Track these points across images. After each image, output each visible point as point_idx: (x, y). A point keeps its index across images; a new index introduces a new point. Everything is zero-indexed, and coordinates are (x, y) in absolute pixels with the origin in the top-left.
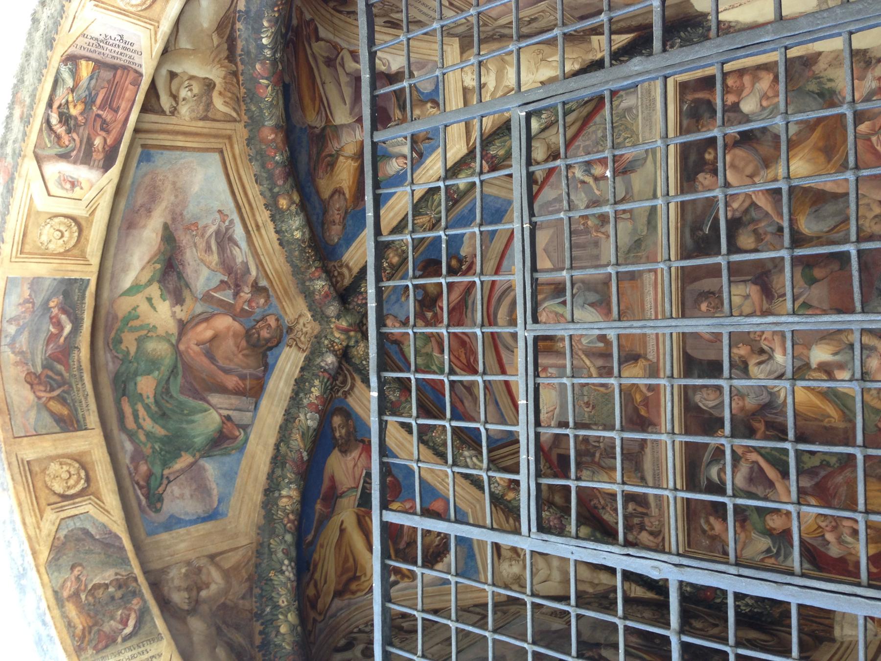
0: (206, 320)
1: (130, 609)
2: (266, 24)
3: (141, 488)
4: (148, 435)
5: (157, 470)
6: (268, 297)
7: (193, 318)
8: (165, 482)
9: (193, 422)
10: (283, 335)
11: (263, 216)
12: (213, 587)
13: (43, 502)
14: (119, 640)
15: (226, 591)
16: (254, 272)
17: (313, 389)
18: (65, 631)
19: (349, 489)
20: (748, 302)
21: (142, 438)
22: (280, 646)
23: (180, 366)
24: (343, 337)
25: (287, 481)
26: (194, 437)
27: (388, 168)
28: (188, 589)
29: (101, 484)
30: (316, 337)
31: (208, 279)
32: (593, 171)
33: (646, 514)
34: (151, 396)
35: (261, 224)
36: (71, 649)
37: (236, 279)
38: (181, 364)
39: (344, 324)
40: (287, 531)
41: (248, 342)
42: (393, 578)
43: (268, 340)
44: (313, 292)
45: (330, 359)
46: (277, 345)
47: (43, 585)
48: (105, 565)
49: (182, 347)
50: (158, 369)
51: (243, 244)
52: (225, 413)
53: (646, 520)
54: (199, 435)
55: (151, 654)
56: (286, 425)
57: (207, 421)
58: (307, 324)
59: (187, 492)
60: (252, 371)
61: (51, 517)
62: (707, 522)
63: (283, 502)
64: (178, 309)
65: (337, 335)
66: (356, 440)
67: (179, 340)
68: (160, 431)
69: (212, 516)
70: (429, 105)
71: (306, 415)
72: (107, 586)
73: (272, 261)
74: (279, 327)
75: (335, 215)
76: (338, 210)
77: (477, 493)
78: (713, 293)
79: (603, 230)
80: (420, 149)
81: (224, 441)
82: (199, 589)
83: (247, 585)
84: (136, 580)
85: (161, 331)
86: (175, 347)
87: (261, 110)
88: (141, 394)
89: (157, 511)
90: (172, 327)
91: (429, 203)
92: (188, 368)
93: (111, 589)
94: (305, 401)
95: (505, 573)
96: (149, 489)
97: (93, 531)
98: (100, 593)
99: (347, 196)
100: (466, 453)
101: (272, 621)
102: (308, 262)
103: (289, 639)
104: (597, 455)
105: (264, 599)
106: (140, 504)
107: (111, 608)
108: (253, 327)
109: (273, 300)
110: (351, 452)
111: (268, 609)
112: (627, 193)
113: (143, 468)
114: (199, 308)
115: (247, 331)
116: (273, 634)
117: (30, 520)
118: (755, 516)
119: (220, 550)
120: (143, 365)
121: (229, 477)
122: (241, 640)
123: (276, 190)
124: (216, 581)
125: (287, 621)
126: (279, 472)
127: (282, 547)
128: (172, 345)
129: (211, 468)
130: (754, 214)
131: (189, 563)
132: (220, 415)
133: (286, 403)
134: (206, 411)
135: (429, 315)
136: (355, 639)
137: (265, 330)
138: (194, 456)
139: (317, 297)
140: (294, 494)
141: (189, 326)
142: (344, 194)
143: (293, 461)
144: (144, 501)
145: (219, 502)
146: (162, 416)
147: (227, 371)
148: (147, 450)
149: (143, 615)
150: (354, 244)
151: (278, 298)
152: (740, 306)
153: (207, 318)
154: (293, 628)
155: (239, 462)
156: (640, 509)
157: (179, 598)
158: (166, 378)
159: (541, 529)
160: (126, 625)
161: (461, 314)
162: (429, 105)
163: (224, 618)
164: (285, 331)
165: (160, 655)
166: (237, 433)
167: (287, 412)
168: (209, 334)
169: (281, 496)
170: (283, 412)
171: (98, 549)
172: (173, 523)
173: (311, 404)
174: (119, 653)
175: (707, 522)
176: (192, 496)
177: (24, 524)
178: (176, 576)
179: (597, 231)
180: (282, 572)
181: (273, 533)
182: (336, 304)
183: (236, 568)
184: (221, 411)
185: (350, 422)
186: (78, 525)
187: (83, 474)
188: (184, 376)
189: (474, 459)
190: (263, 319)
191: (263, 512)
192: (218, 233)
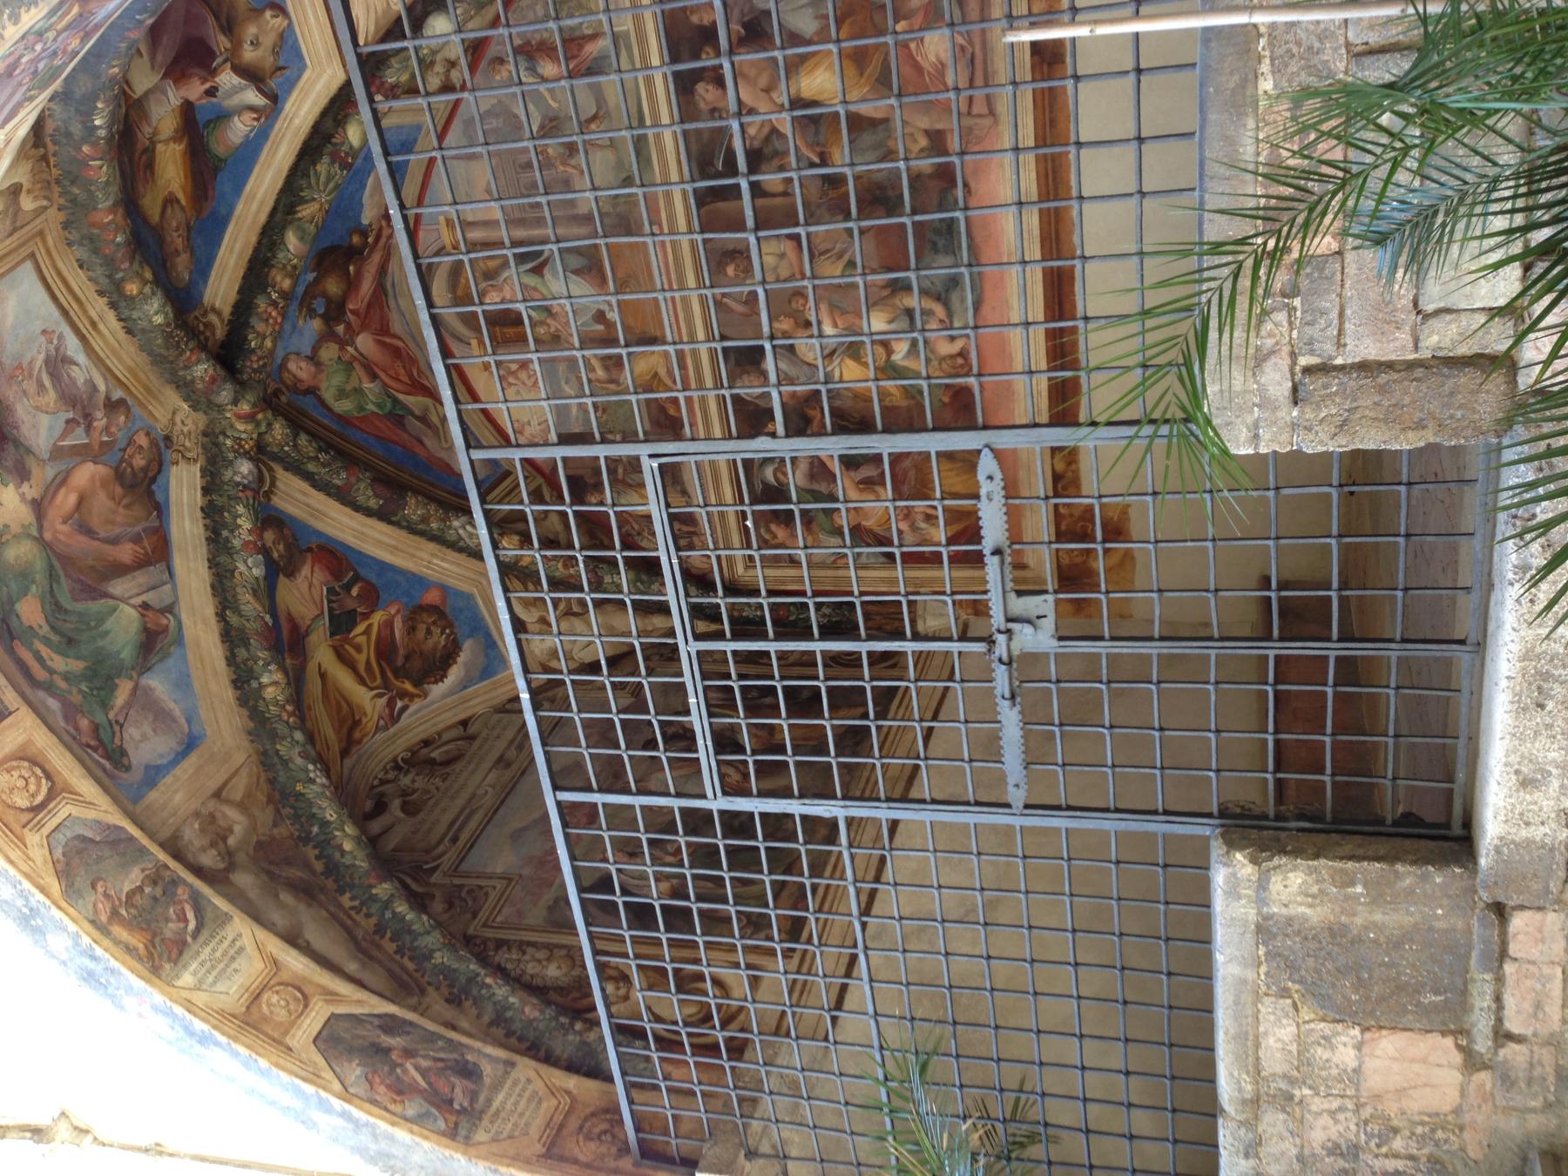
0: (64, 482)
1: (181, 902)
2: (100, 105)
3: (95, 749)
4: (66, 677)
5: (100, 718)
6: (128, 409)
7: (47, 488)
8: (117, 728)
9: (107, 633)
10: (162, 449)
11: (98, 306)
12: (237, 829)
13: (16, 827)
14: (189, 939)
15: (253, 828)
16: (102, 387)
17: (239, 521)
18: (128, 957)
19: (313, 620)
20: (784, 263)
21: (63, 684)
22: (353, 866)
23: (56, 563)
24: (250, 427)
25: (261, 663)
26: (119, 652)
27: (231, 136)
28: (213, 844)
29: (66, 774)
30: (205, 434)
31: (50, 428)
32: (540, 70)
33: (694, 533)
34: (42, 622)
35: (96, 318)
36: (146, 973)
37: (84, 408)
38: (59, 561)
39: (245, 407)
40: (292, 729)
41: (122, 485)
42: (399, 704)
43: (145, 469)
44: (193, 381)
45: (245, 467)
46: (159, 471)
47: (73, 919)
48: (125, 866)
49: (48, 536)
50: (33, 582)
51: (81, 358)
52: (138, 601)
53: (695, 539)
54: (123, 647)
55: (230, 938)
56: (221, 582)
57: (124, 625)
58: (186, 421)
59: (147, 728)
60: (145, 524)
61: (34, 839)
62: (769, 531)
63: (270, 693)
64: (25, 487)
65: (241, 427)
66: (301, 552)
67: (40, 528)
68: (77, 666)
69: (190, 744)
70: (268, 14)
71: (245, 562)
72: (140, 889)
73: (120, 360)
74: (153, 443)
75: (176, 240)
76: (177, 229)
77: (472, 563)
78: (740, 252)
79: (573, 162)
80: (271, 89)
81: (155, 640)
82: (224, 839)
83: (271, 807)
84: (166, 867)
85: (15, 528)
86: (40, 540)
87: (91, 194)
88: (31, 627)
89: (128, 768)
90: (25, 514)
91: (313, 181)
92: (67, 560)
93: (147, 890)
94: (236, 543)
95: (537, 651)
96: (105, 748)
97: (89, 834)
98: (137, 899)
99: (183, 202)
100: (456, 523)
101: (328, 842)
102: (178, 346)
103: (360, 854)
104: (620, 471)
105: (303, 819)
106: (105, 770)
107: (160, 910)
108: (122, 460)
109: (136, 410)
110: (299, 570)
111: (315, 829)
112: (599, 108)
113: (84, 723)
114: (50, 472)
115: (116, 470)
116: (337, 855)
117: (15, 855)
118: (821, 517)
119: (221, 781)
120: (13, 586)
121: (183, 683)
122: (299, 874)
123: (120, 275)
124: (237, 822)
125: (348, 836)
126: (242, 653)
127: (297, 750)
128: (36, 539)
129: (157, 683)
130: (777, 144)
131: (197, 815)
132: (134, 607)
133: (204, 550)
134: (115, 610)
135: (340, 329)
136: (382, 795)
137: (138, 457)
138: (131, 678)
139: (200, 386)
140: (279, 677)
141: (46, 502)
142: (178, 201)
143: (257, 633)
144: (107, 765)
145: (189, 721)
146: (69, 643)
147: (114, 541)
148: (76, 699)
149: (197, 901)
150: (213, 273)
151: (141, 404)
152: (775, 269)
153: (63, 480)
154: (358, 841)
155: (185, 661)
156: (685, 529)
157: (209, 859)
158: (47, 589)
159: (725, 793)
160: (186, 921)
161: (382, 308)
162: (268, 14)
163: (272, 859)
164: (162, 445)
165: (240, 935)
166: (165, 622)
167: (213, 563)
168: (72, 499)
169: (262, 687)
170: (206, 564)
171: (107, 853)
172: (153, 775)
173: (246, 544)
174: (198, 953)
175: (769, 531)
176: (154, 731)
177: (11, 862)
178: (192, 835)
179: (564, 164)
180: (313, 781)
181: (274, 736)
182: (228, 386)
183: (248, 794)
184: (133, 601)
185: (286, 531)
186: (69, 834)
187: (39, 772)
188: (68, 576)
189: (468, 528)
190: (130, 442)
191: (245, 712)
192: (47, 361)
